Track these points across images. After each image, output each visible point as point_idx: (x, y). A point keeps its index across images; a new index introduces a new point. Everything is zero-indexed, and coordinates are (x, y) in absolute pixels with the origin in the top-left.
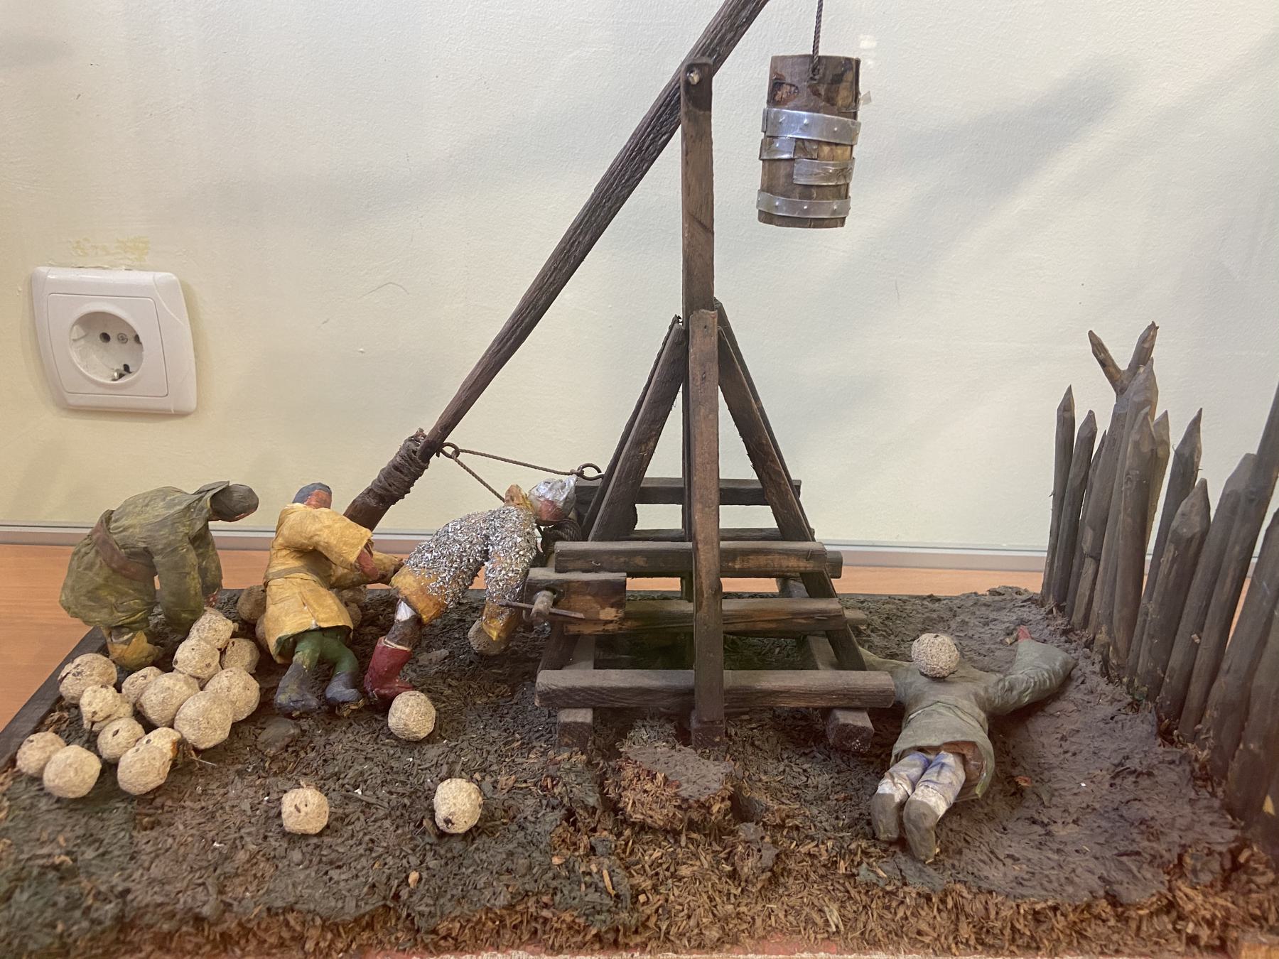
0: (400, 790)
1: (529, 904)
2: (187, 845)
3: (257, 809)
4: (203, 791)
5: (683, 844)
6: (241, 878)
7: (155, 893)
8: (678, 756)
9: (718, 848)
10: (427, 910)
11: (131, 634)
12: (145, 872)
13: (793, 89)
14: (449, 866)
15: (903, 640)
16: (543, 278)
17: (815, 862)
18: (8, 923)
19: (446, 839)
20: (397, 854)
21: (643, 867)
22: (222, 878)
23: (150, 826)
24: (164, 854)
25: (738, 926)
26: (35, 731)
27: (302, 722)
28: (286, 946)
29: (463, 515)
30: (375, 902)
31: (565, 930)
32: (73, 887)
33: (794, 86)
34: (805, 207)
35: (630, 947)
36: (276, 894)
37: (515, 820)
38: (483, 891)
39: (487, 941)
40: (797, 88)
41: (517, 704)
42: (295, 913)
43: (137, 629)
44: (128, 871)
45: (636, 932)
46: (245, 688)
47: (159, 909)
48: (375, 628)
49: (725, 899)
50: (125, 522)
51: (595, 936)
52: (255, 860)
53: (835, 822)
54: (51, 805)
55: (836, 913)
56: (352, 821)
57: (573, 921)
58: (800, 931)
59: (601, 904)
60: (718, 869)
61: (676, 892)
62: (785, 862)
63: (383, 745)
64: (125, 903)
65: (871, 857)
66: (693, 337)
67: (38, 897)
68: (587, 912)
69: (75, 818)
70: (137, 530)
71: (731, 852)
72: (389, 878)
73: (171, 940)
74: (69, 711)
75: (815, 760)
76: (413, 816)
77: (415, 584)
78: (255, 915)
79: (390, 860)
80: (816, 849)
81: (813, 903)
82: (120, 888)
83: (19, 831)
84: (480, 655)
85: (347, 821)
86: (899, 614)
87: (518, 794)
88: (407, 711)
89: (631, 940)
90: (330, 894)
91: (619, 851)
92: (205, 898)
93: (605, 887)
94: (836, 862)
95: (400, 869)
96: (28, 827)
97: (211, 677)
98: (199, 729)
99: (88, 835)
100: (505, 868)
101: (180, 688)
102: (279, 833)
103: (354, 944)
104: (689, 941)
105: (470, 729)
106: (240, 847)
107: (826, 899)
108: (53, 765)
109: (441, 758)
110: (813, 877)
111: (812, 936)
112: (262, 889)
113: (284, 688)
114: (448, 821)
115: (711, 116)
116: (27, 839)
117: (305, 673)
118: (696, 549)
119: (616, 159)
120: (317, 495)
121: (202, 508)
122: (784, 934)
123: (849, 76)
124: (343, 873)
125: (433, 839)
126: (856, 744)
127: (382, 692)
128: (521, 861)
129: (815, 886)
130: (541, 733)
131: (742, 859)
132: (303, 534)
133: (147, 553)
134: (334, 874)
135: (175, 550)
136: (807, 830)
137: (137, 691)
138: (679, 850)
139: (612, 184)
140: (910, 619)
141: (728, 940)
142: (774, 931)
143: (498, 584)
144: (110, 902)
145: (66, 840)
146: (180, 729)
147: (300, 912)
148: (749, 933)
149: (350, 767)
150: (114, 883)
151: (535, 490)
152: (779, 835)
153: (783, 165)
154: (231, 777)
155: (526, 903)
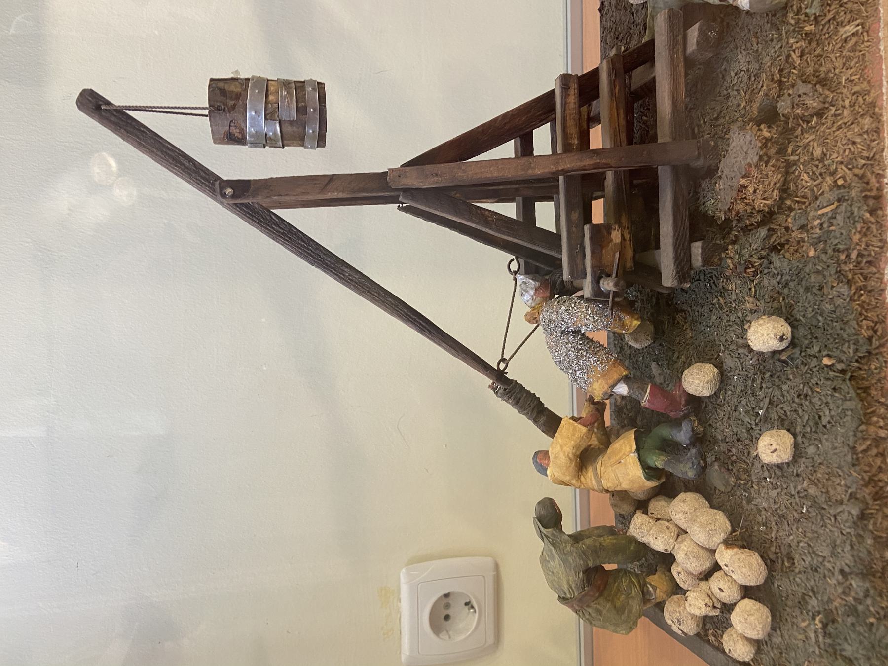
0: (759, 381)
1: (847, 269)
2: (805, 531)
3: (776, 484)
4: (763, 526)
5: (797, 158)
6: (830, 489)
7: (843, 550)
8: (726, 171)
9: (800, 129)
10: (852, 347)
11: (649, 586)
12: (827, 560)
13: (232, 124)
14: (818, 335)
15: (634, 23)
16: (376, 300)
17: (806, 51)
18: (869, 659)
19: (796, 341)
20: (809, 376)
21: (815, 186)
22: (829, 503)
23: (792, 561)
24: (812, 548)
25: (861, 104)
26: (723, 652)
27: (709, 460)
28: (884, 452)
29: (548, 352)
30: (848, 388)
31: (867, 239)
32: (840, 612)
33: (230, 124)
34: (312, 110)
35: (880, 186)
36: (842, 461)
37: (781, 291)
38: (836, 305)
39: (877, 299)
40: (231, 121)
41: (691, 307)
42: (856, 446)
43: (645, 581)
44: (826, 572)
45: (868, 183)
46: (684, 501)
47: (855, 547)
48: (638, 419)
49: (839, 118)
50: (566, 587)
51: (871, 215)
52: (816, 481)
53: (775, 41)
54: (778, 635)
55: (847, 28)
56: (783, 412)
57: (860, 232)
58: (863, 55)
59: (845, 212)
60: (815, 128)
61: (834, 156)
62: (808, 76)
63: (724, 400)
64: (851, 573)
65: (800, 7)
66: (407, 185)
67: (848, 638)
68: (852, 222)
69: (787, 617)
70: (571, 578)
71: (801, 119)
72: (828, 379)
73: (880, 537)
74: (709, 630)
75: (728, 69)
76: (779, 369)
77: (600, 381)
78: (859, 474)
79: (813, 381)
80: (796, 51)
81: (840, 48)
82: (840, 577)
83: (798, 655)
84: (655, 340)
85: (784, 417)
86: (613, 30)
87: (760, 293)
88: (697, 382)
89: (874, 186)
90: (841, 421)
91: (803, 207)
92: (846, 514)
93: (832, 210)
94: (806, 34)
95: (820, 372)
96: (794, 650)
97: (677, 526)
98: (715, 530)
99: (800, 605)
100: (818, 292)
101: (685, 546)
102: (794, 466)
103: (880, 400)
104: (874, 140)
105: (711, 337)
106: (806, 493)
107: (836, 38)
108: (746, 631)
109: (733, 355)
110: (819, 51)
111: (866, 44)
112: (837, 472)
113: (683, 473)
114: (782, 339)
115: (254, 180)
116: (803, 650)
117: (671, 459)
118: (564, 172)
119: (290, 250)
120: (541, 459)
121: (553, 534)
122: (866, 67)
123: (221, 85)
124: (824, 413)
125: (797, 351)
126: (712, 35)
127: (683, 402)
128: (813, 279)
129: (826, 48)
130: (712, 284)
131: (807, 108)
132: (568, 465)
133: (588, 572)
134: (825, 421)
135: (584, 553)
136: (782, 63)
137: (690, 578)
138: (802, 160)
139: (308, 253)
140: (617, 21)
141: (872, 110)
142: (863, 76)
143: (597, 320)
144: (851, 584)
145: (804, 620)
146: (716, 544)
147: (856, 442)
148: (866, 95)
149: (742, 421)
150: (835, 582)
151: (528, 303)
152: (787, 84)
153: (285, 129)
154: (753, 507)
155: (846, 271)
